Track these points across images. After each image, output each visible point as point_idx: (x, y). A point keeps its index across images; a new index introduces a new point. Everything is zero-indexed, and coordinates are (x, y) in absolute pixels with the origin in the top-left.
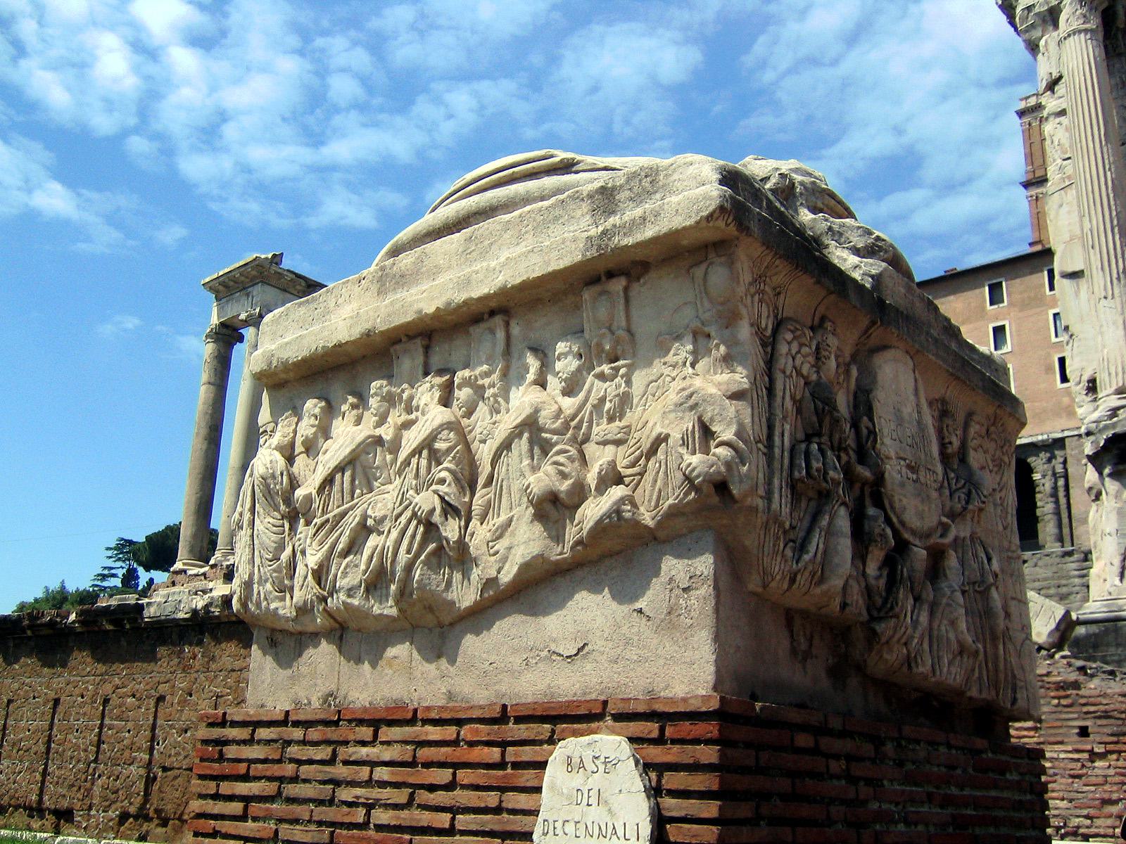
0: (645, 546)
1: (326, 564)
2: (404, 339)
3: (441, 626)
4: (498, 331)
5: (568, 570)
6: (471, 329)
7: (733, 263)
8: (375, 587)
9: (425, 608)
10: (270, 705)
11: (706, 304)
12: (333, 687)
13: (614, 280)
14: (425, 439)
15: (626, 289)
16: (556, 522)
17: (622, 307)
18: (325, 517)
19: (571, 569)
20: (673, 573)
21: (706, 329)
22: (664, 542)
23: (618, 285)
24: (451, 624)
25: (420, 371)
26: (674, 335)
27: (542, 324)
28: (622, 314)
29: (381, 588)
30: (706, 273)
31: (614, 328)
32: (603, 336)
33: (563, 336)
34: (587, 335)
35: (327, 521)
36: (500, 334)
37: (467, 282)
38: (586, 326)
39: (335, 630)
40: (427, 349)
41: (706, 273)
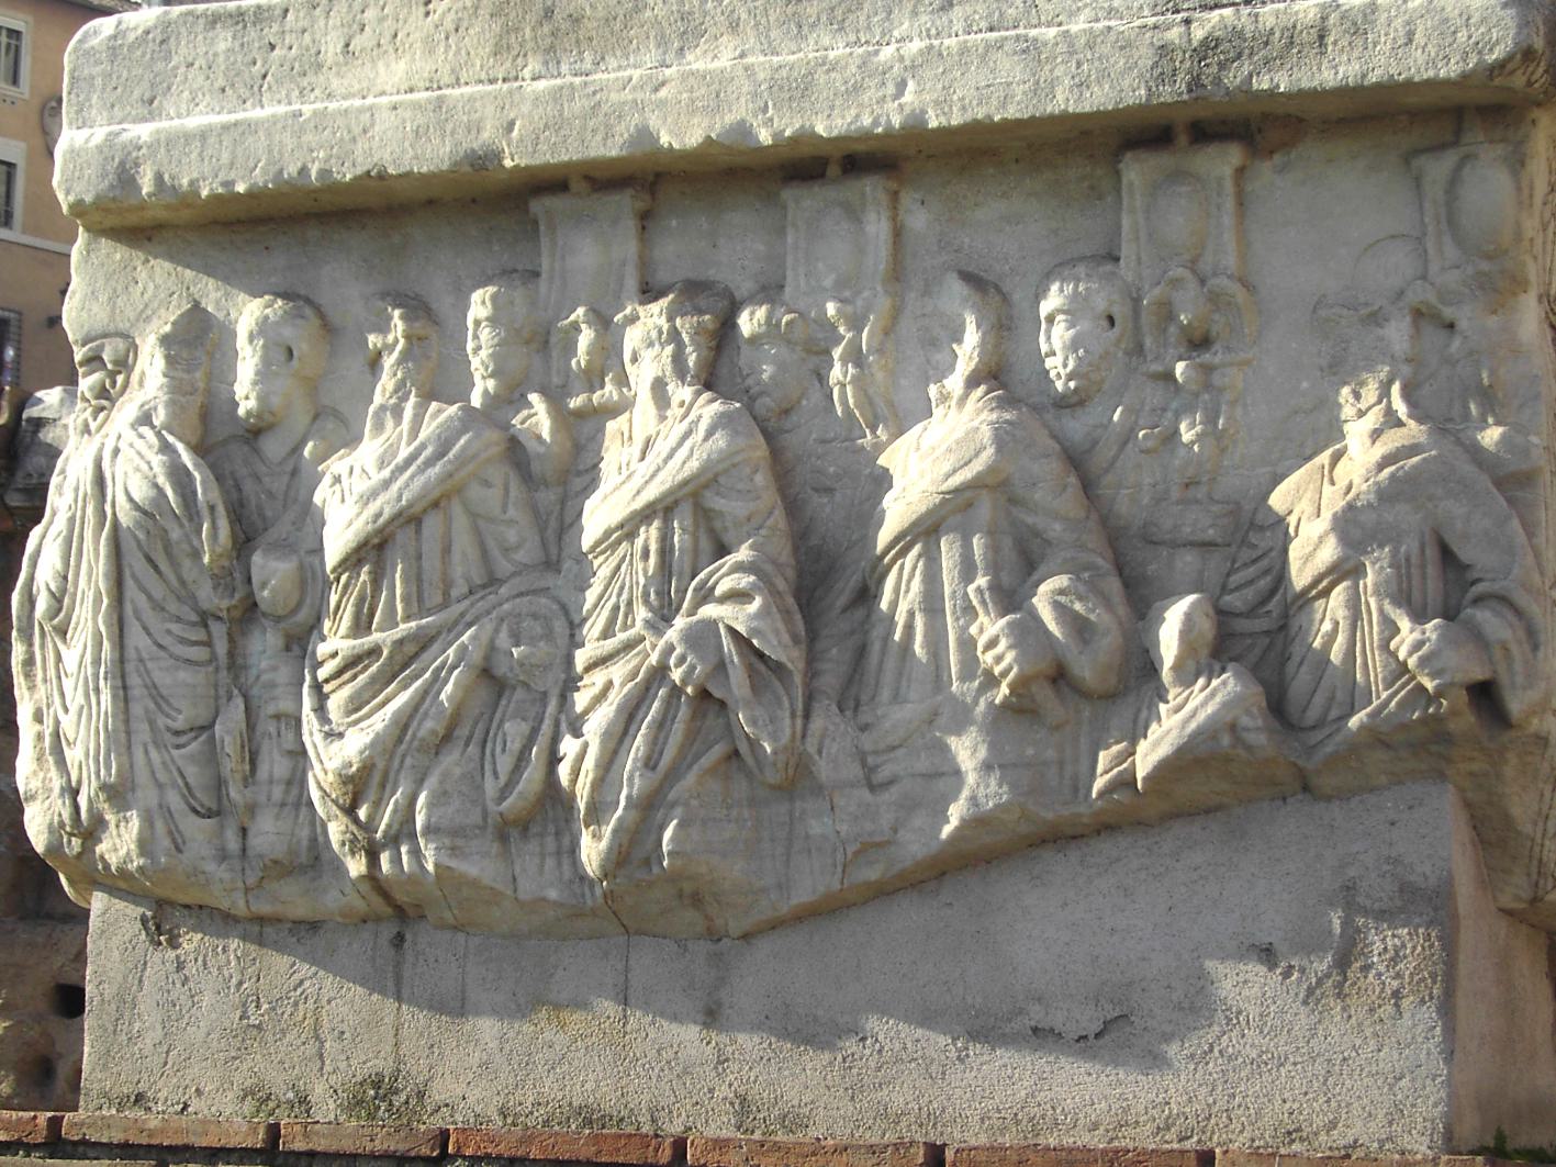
0: (1280, 803)
1: (381, 765)
2: (575, 185)
3: (713, 935)
4: (871, 216)
5: (1074, 838)
6: (788, 194)
7: (1522, 164)
8: (525, 829)
9: (680, 895)
10: (165, 1094)
11: (1451, 252)
12: (383, 1064)
13: (1213, 150)
14: (685, 483)
15: (1240, 172)
16: (1058, 728)
17: (1228, 220)
18: (367, 642)
19: (1082, 836)
20: (1352, 872)
21: (1448, 312)
22: (1329, 799)
23: (1222, 161)
24: (746, 937)
25: (631, 283)
26: (1364, 312)
27: (1003, 223)
28: (1229, 238)
29: (542, 835)
30: (1454, 181)
31: (1205, 266)
32: (1176, 283)
33: (1058, 268)
34: (1126, 269)
35: (374, 652)
36: (877, 227)
37: (797, 89)
38: (1127, 251)
39: (378, 919)
40: (645, 218)
41: (1454, 181)
